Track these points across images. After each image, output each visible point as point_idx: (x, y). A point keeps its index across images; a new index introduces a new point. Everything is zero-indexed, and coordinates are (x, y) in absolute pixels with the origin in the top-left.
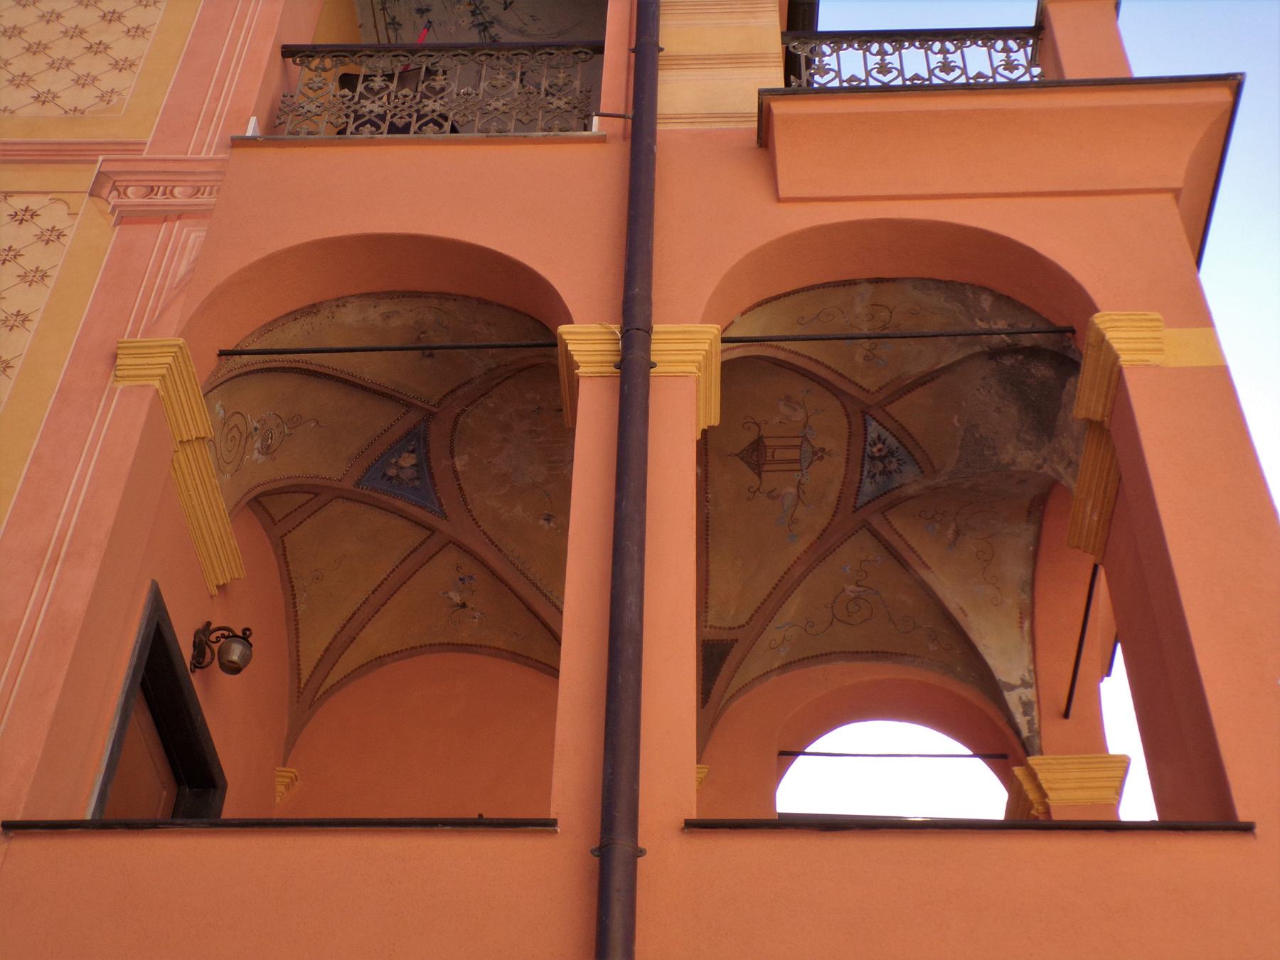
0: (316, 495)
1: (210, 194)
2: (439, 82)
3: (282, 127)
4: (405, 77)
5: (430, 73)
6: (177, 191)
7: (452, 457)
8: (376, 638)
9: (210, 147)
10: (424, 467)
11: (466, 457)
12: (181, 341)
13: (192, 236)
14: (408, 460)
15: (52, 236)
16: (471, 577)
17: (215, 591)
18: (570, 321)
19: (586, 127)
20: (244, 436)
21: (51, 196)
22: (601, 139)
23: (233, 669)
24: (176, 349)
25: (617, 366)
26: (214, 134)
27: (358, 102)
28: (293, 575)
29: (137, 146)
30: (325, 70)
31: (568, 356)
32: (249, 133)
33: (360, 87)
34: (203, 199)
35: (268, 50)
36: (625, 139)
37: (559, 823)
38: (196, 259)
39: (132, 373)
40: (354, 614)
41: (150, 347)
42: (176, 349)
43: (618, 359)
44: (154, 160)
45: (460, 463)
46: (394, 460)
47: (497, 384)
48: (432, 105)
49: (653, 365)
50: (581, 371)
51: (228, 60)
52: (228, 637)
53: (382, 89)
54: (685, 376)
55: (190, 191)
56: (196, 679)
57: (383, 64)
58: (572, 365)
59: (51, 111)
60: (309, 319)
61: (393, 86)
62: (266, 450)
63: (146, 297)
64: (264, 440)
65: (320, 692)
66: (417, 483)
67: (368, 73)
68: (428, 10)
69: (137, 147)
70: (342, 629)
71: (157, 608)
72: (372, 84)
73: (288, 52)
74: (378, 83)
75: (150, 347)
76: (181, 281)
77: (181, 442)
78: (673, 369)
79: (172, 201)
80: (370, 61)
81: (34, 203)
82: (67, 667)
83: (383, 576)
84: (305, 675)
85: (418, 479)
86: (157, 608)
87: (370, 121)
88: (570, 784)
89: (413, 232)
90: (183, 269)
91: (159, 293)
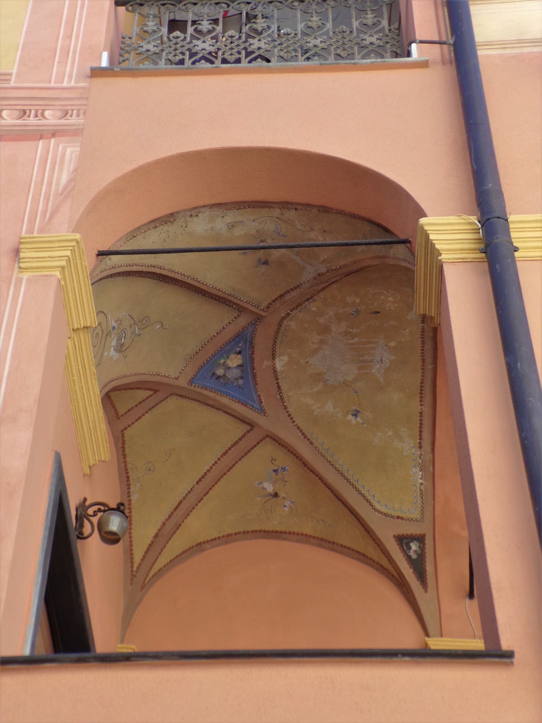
0: (156, 391)
1: (78, 115)
2: (260, 24)
5: (250, 18)
6: (47, 113)
7: (274, 358)
8: (199, 525)
9: (70, 77)
10: (248, 369)
11: (286, 358)
12: (78, 236)
13: (69, 150)
14: (234, 361)
16: (284, 469)
18: (424, 215)
19: (409, 54)
20: (105, 334)
22: (423, 65)
24: (73, 243)
27: (190, 42)
28: (129, 466)
33: (190, 30)
36: (451, 62)
37: (516, 654)
38: (76, 170)
40: (180, 503)
42: (73, 243)
43: (482, 246)
44: (22, 88)
46: (222, 361)
47: (323, 289)
48: (255, 43)
50: (444, 257)
52: (104, 511)
53: (210, 32)
55: (59, 114)
60: (166, 228)
61: (219, 28)
62: (120, 348)
63: (36, 201)
64: (119, 339)
65: (150, 575)
66: (241, 382)
67: (196, 18)
70: (170, 517)
72: (200, 27)
76: (65, 188)
77: (73, 330)
79: (44, 122)
80: (196, 8)
82: (17, 518)
83: (207, 468)
84: (137, 559)
85: (242, 378)
87: (203, 58)
90: (64, 179)
91: (47, 199)
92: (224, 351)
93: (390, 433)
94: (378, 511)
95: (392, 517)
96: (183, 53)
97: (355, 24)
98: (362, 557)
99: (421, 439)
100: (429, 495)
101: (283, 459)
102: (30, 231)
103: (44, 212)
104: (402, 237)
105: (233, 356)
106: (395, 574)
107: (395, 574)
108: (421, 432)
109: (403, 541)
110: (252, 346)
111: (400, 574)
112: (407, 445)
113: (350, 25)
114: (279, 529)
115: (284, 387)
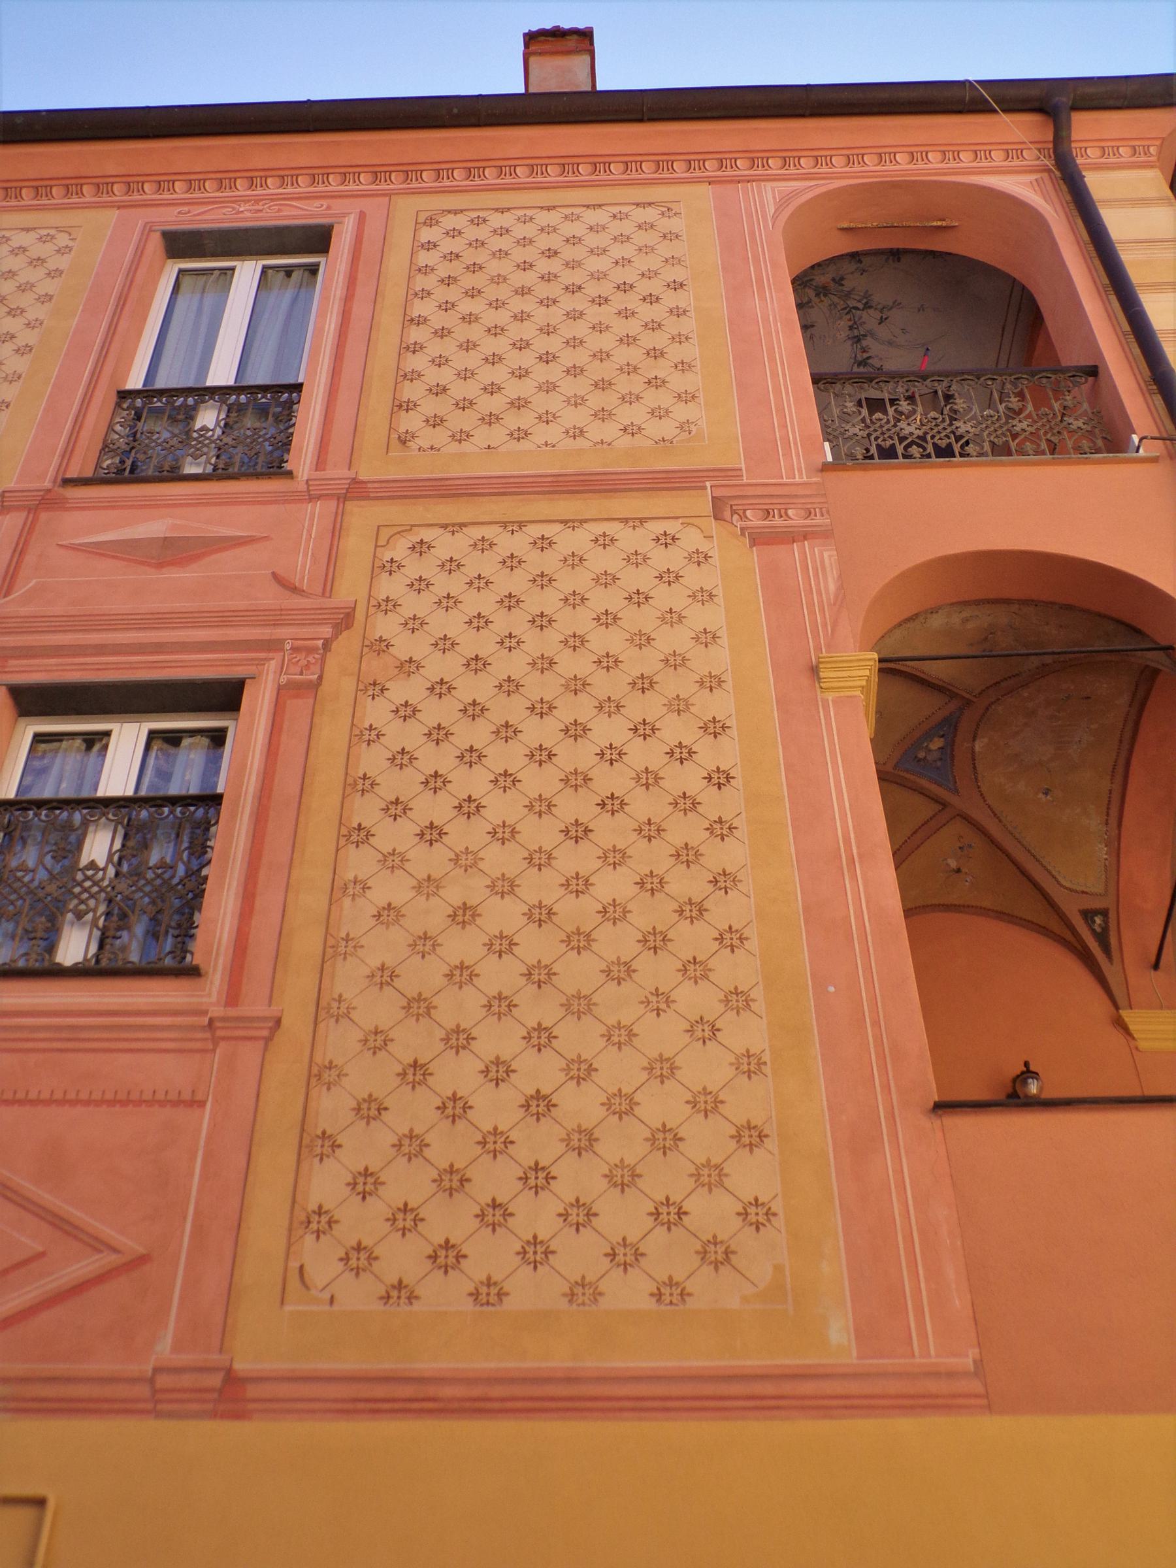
1: (822, 515)
6: (790, 512)
10: (948, 752)
11: (986, 740)
13: (826, 555)
15: (700, 558)
16: (970, 846)
21: (681, 521)
22: (1154, 460)
26: (798, 459)
29: (734, 473)
38: (840, 577)
39: (836, 685)
41: (851, 661)
45: (978, 746)
63: (812, 613)
66: (939, 763)
68: (812, 326)
69: (735, 473)
72: (900, 408)
75: (851, 661)
76: (836, 597)
85: (941, 759)
89: (1023, 548)
90: (832, 587)
91: (822, 610)
92: (928, 735)
93: (1078, 810)
94: (1062, 886)
95: (1076, 892)
96: (891, 438)
97: (1056, 406)
98: (1044, 931)
99: (1108, 815)
100: (1114, 867)
102: (818, 648)
103: (825, 625)
104: (1164, 643)
105: (936, 739)
106: (1079, 947)
107: (1079, 947)
108: (1108, 808)
109: (1088, 915)
111: (1086, 948)
112: (1094, 823)
113: (1051, 408)
114: (956, 903)
115: (980, 768)
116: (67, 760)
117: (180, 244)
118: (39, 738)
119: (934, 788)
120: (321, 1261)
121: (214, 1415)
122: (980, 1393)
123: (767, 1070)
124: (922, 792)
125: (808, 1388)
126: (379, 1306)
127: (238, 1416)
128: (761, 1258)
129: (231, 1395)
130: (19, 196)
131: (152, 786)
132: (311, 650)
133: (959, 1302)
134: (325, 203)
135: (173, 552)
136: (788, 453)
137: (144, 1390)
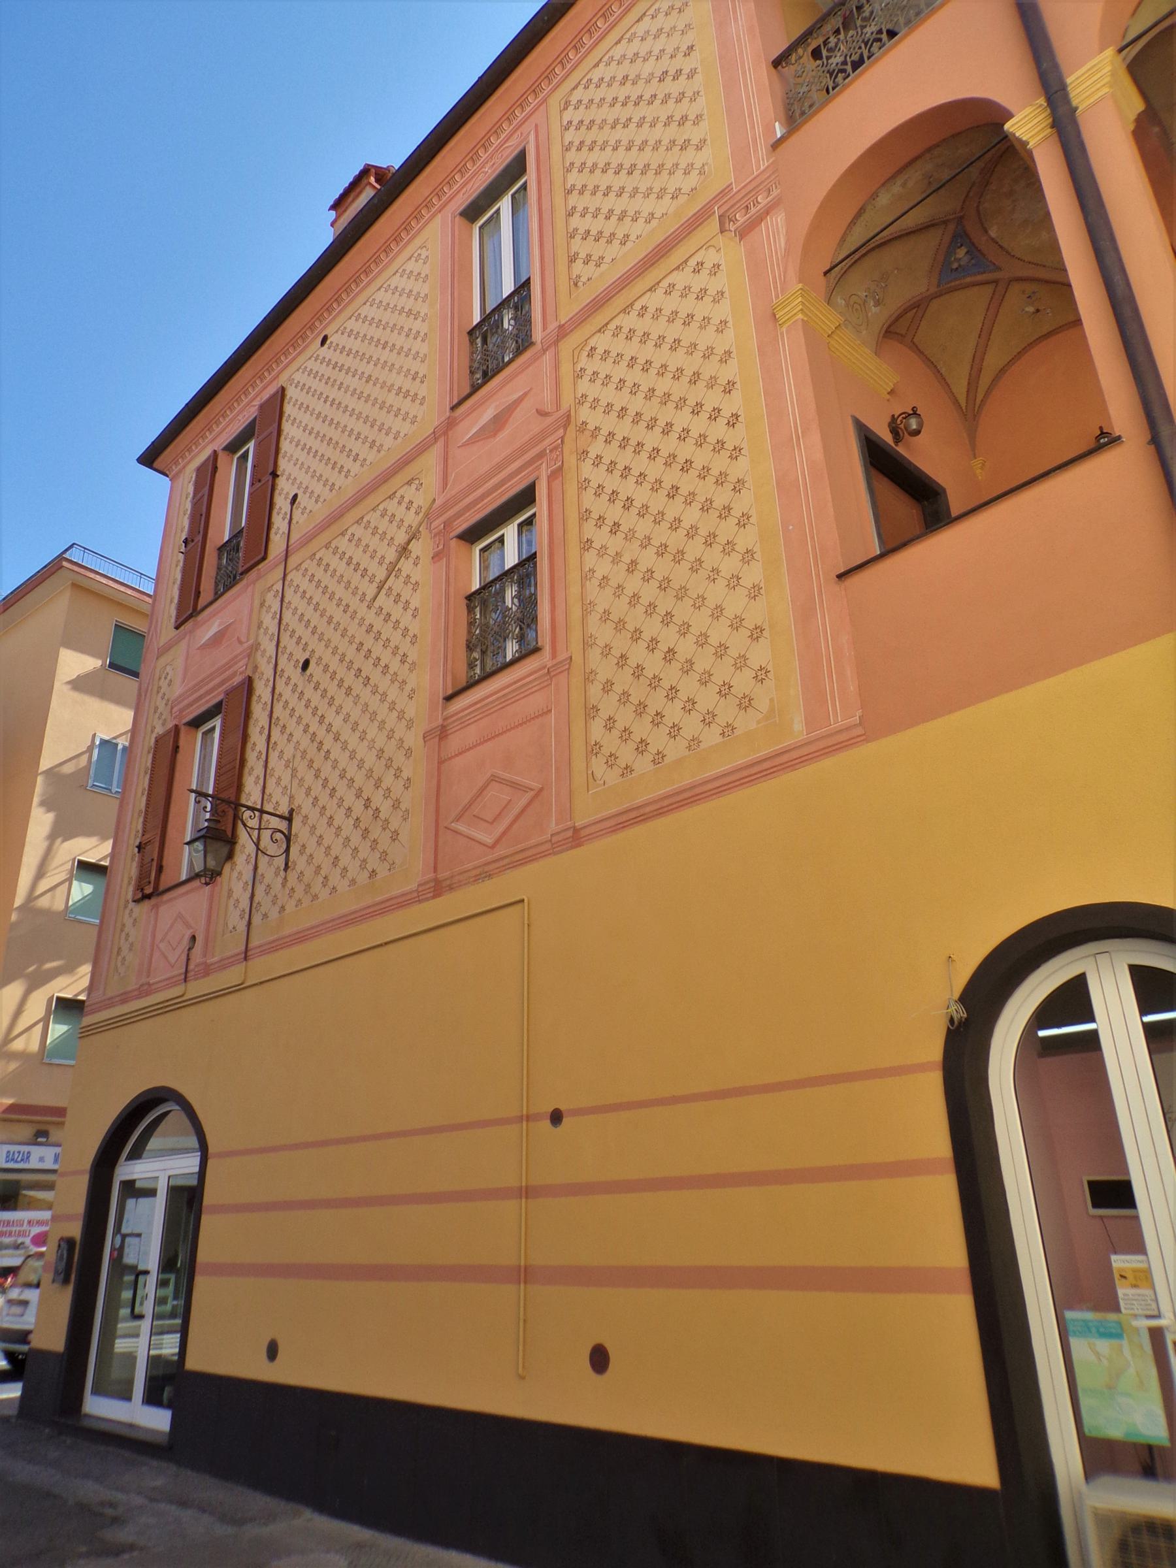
3: (796, 113)
4: (847, 24)
7: (986, 232)
8: (993, 360)
11: (995, 227)
12: (800, 286)
14: (961, 253)
17: (888, 397)
23: (917, 432)
25: (1052, 127)
30: (800, 58)
31: (1019, 140)
32: (779, 135)
33: (824, 53)
34: (775, 193)
35: (764, 71)
45: (993, 233)
49: (1076, 108)
51: (748, 98)
53: (836, 44)
54: (1102, 99)
55: (765, 194)
56: (901, 449)
57: (828, 28)
58: (1024, 144)
59: (682, 199)
62: (878, 303)
71: (861, 427)
73: (777, 63)
74: (833, 40)
78: (1096, 97)
81: (698, 258)
84: (963, 405)
86: (861, 427)
88: (1121, 408)
90: (783, 245)
91: (778, 265)
92: (950, 251)
101: (1029, 288)
110: (967, 236)
115: (1005, 245)
116: (494, 557)
117: (472, 212)
118: (483, 550)
119: (979, 278)
120: (598, 765)
121: (572, 848)
122: (873, 726)
123: (762, 591)
124: (974, 284)
125: (785, 758)
126: (621, 779)
127: (579, 845)
128: (763, 699)
129: (577, 838)
130: (343, 300)
131: (528, 551)
132: (556, 448)
133: (852, 688)
134: (519, 132)
135: (499, 422)
136: (756, 151)
137: (548, 846)
